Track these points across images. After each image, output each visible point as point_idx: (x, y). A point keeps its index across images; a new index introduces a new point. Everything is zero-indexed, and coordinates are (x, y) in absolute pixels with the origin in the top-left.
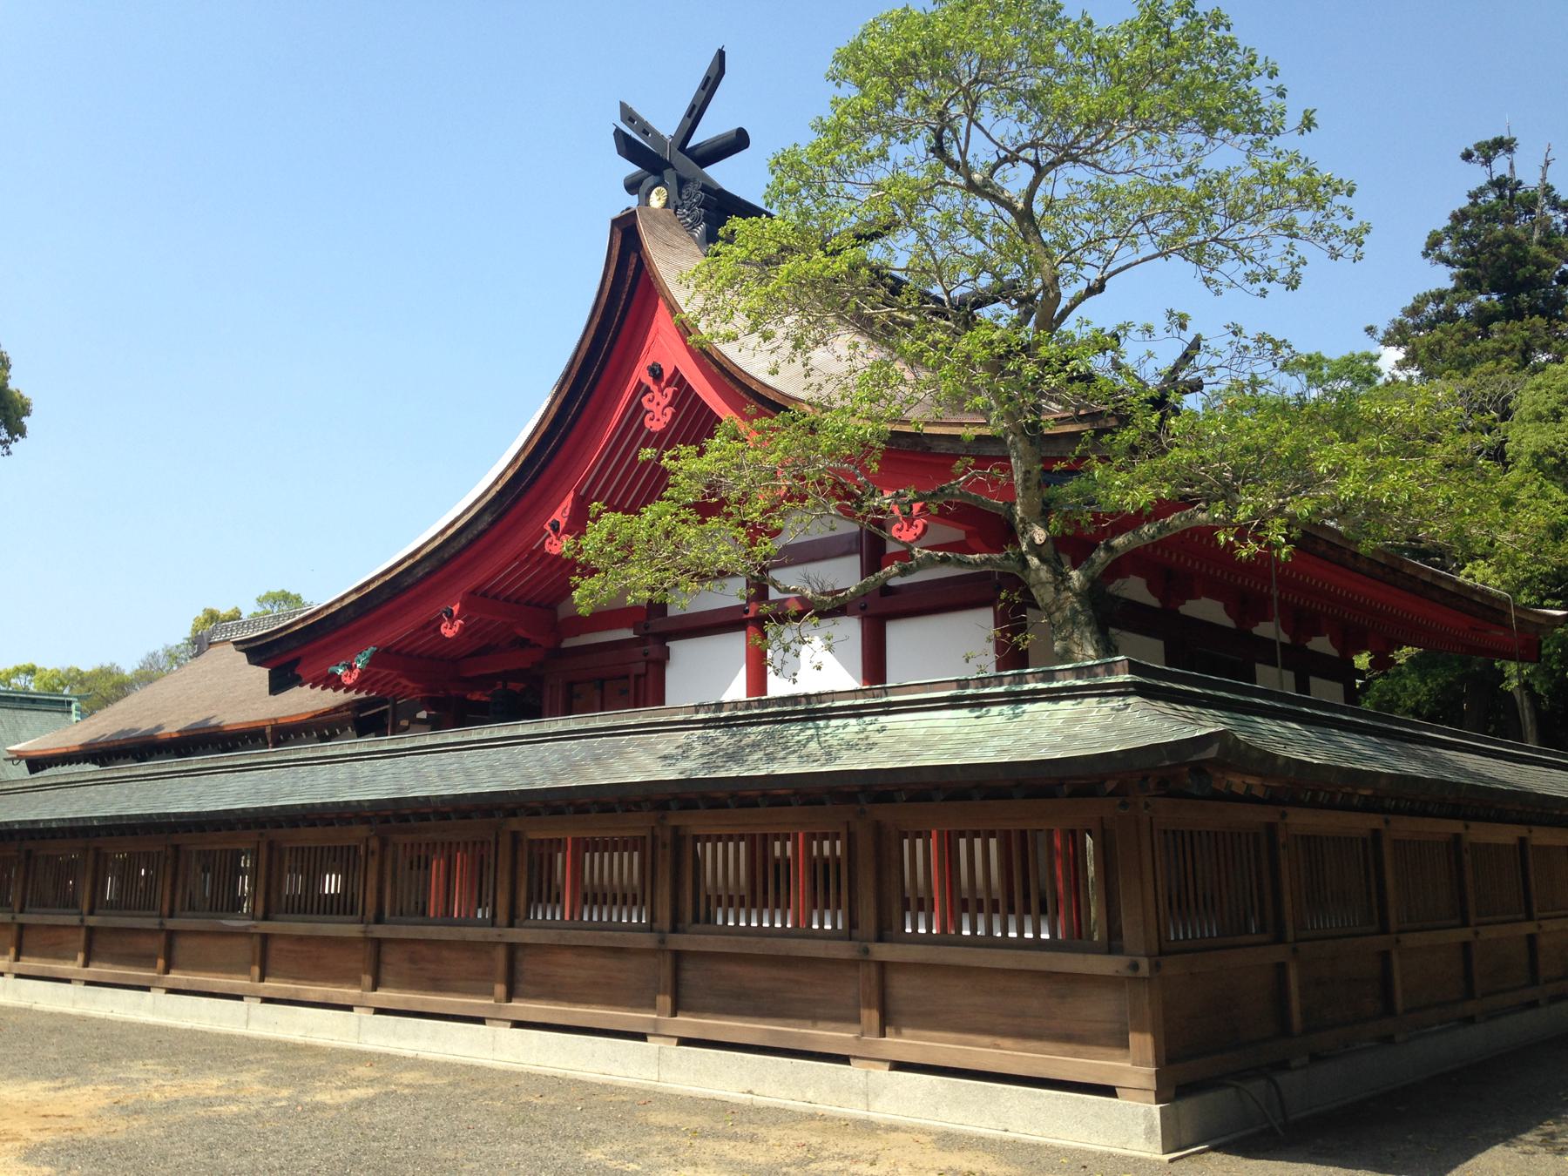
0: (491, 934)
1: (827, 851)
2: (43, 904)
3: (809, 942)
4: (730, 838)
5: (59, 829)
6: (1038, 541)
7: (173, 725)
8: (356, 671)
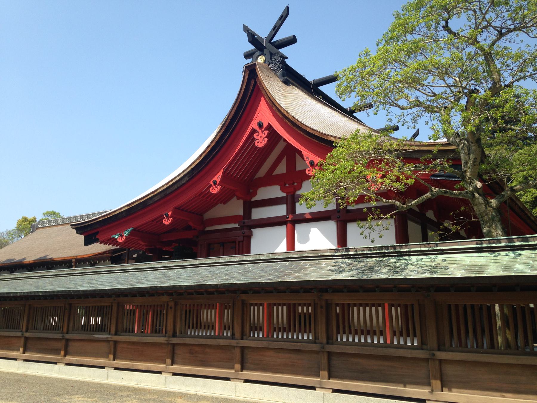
0: (233, 342)
1: (305, 311)
2: (35, 328)
3: (201, 340)
4: (279, 305)
5: (19, 296)
6: (478, 187)
7: (30, 258)
8: (124, 237)
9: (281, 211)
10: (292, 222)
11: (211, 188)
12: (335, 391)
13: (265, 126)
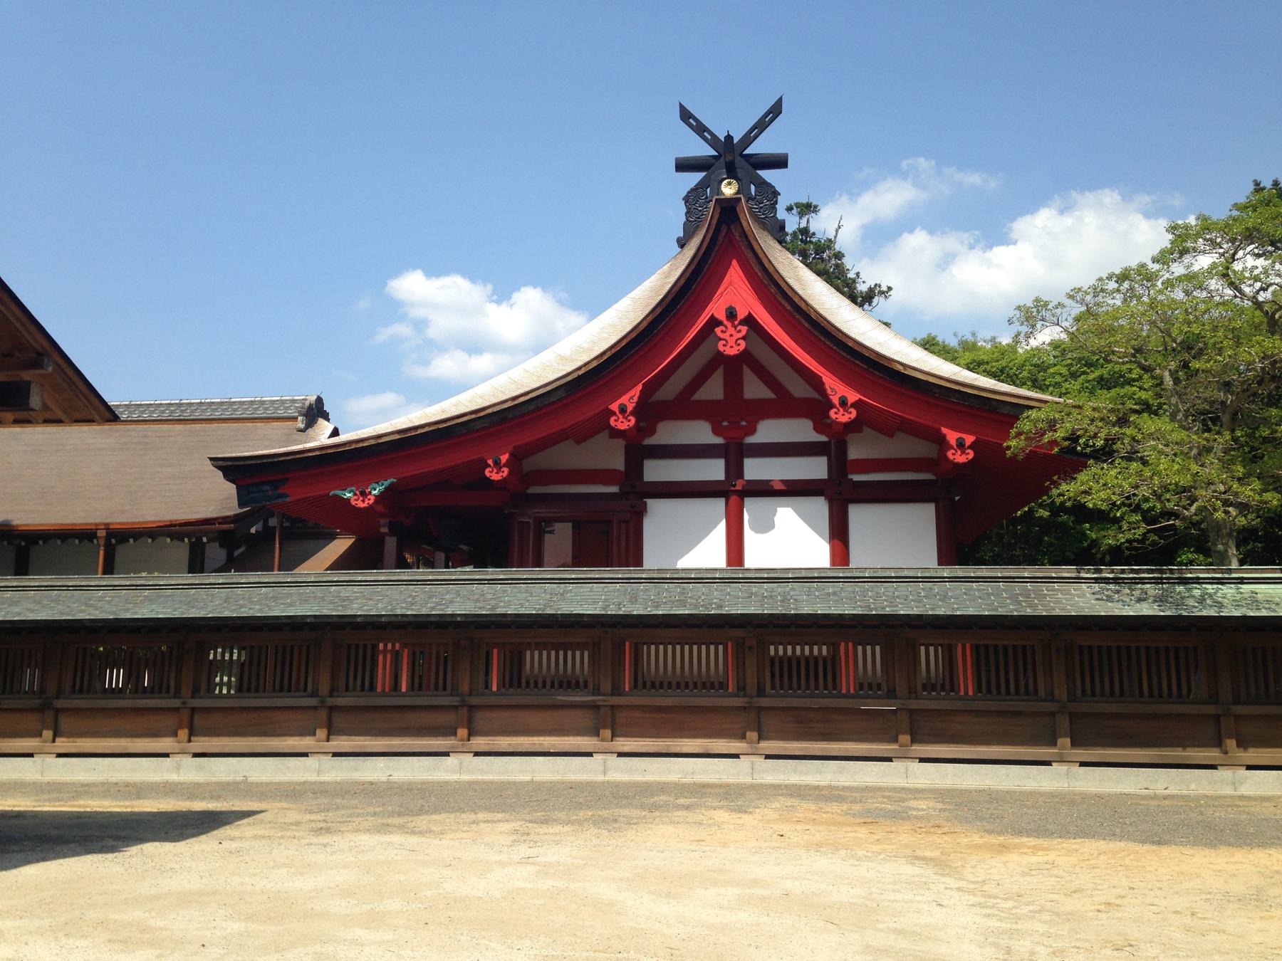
9: (714, 470)
10: (735, 494)
11: (613, 418)
12: (1083, 764)
13: (741, 315)
